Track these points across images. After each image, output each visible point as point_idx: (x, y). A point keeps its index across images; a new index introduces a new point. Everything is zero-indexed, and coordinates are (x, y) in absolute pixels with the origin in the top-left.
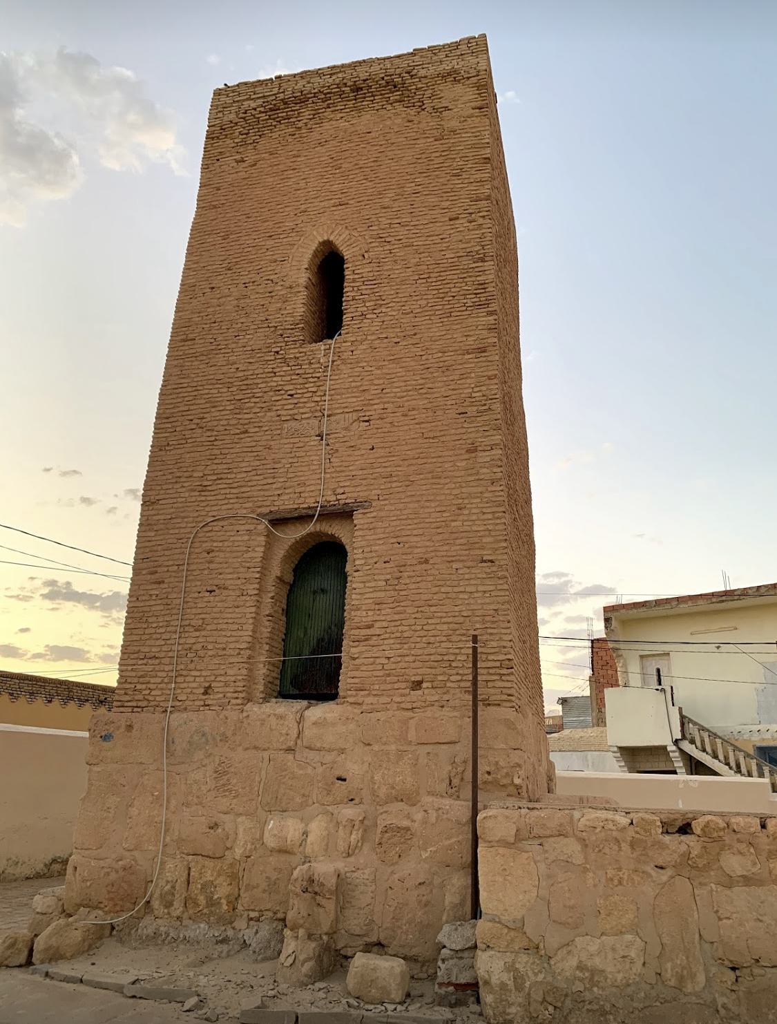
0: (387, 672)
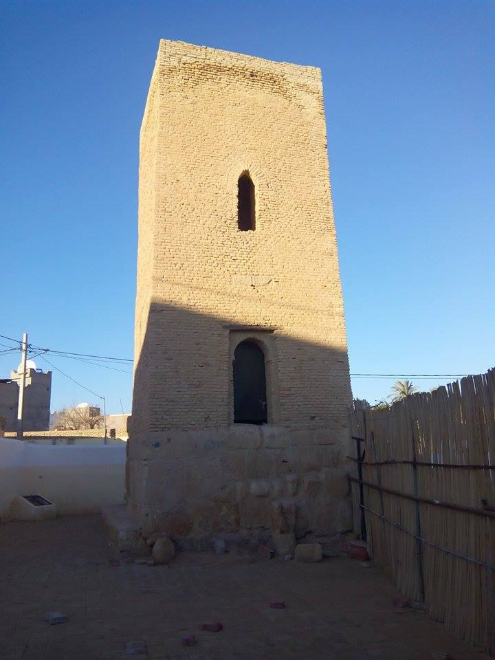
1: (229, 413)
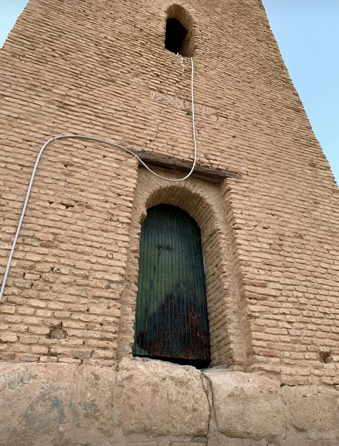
0: (294, 338)
1: (119, 323)
